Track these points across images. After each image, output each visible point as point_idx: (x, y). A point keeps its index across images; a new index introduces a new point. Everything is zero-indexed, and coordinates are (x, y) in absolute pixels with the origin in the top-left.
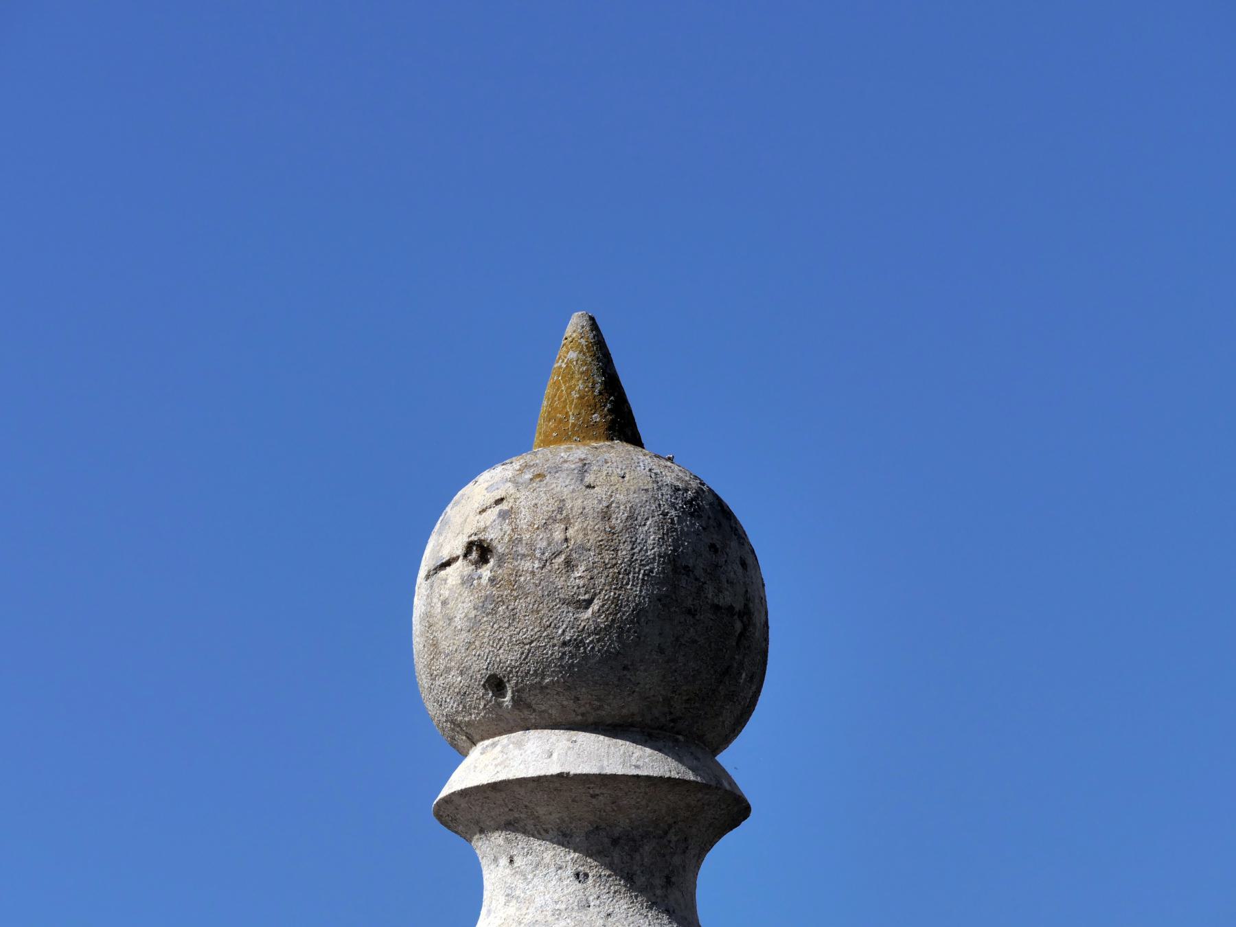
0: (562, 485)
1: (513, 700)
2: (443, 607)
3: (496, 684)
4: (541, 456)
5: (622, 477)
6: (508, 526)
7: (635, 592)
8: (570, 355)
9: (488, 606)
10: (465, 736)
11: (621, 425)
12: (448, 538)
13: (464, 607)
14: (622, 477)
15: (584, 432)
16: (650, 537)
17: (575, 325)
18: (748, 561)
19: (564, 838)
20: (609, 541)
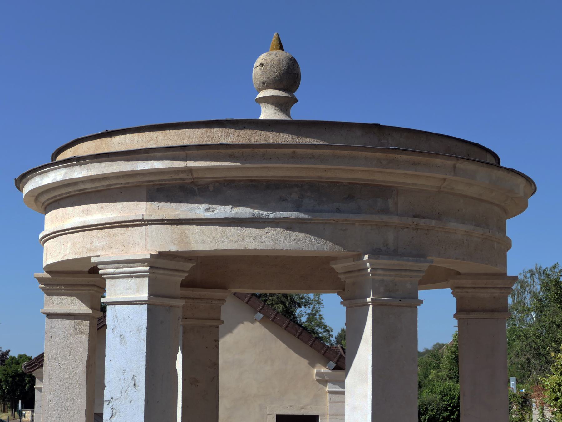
0: (273, 56)
1: (266, 85)
2: (257, 72)
3: (264, 83)
4: (270, 52)
5: (281, 55)
6: (265, 62)
7: (283, 71)
8: (274, 38)
9: (263, 72)
10: (259, 90)
11: (281, 48)
12: (257, 63)
13: (259, 73)
14: (281, 55)
15: (276, 49)
16: (285, 64)
17: (275, 34)
18: (298, 67)
19: (272, 104)
20: (280, 64)
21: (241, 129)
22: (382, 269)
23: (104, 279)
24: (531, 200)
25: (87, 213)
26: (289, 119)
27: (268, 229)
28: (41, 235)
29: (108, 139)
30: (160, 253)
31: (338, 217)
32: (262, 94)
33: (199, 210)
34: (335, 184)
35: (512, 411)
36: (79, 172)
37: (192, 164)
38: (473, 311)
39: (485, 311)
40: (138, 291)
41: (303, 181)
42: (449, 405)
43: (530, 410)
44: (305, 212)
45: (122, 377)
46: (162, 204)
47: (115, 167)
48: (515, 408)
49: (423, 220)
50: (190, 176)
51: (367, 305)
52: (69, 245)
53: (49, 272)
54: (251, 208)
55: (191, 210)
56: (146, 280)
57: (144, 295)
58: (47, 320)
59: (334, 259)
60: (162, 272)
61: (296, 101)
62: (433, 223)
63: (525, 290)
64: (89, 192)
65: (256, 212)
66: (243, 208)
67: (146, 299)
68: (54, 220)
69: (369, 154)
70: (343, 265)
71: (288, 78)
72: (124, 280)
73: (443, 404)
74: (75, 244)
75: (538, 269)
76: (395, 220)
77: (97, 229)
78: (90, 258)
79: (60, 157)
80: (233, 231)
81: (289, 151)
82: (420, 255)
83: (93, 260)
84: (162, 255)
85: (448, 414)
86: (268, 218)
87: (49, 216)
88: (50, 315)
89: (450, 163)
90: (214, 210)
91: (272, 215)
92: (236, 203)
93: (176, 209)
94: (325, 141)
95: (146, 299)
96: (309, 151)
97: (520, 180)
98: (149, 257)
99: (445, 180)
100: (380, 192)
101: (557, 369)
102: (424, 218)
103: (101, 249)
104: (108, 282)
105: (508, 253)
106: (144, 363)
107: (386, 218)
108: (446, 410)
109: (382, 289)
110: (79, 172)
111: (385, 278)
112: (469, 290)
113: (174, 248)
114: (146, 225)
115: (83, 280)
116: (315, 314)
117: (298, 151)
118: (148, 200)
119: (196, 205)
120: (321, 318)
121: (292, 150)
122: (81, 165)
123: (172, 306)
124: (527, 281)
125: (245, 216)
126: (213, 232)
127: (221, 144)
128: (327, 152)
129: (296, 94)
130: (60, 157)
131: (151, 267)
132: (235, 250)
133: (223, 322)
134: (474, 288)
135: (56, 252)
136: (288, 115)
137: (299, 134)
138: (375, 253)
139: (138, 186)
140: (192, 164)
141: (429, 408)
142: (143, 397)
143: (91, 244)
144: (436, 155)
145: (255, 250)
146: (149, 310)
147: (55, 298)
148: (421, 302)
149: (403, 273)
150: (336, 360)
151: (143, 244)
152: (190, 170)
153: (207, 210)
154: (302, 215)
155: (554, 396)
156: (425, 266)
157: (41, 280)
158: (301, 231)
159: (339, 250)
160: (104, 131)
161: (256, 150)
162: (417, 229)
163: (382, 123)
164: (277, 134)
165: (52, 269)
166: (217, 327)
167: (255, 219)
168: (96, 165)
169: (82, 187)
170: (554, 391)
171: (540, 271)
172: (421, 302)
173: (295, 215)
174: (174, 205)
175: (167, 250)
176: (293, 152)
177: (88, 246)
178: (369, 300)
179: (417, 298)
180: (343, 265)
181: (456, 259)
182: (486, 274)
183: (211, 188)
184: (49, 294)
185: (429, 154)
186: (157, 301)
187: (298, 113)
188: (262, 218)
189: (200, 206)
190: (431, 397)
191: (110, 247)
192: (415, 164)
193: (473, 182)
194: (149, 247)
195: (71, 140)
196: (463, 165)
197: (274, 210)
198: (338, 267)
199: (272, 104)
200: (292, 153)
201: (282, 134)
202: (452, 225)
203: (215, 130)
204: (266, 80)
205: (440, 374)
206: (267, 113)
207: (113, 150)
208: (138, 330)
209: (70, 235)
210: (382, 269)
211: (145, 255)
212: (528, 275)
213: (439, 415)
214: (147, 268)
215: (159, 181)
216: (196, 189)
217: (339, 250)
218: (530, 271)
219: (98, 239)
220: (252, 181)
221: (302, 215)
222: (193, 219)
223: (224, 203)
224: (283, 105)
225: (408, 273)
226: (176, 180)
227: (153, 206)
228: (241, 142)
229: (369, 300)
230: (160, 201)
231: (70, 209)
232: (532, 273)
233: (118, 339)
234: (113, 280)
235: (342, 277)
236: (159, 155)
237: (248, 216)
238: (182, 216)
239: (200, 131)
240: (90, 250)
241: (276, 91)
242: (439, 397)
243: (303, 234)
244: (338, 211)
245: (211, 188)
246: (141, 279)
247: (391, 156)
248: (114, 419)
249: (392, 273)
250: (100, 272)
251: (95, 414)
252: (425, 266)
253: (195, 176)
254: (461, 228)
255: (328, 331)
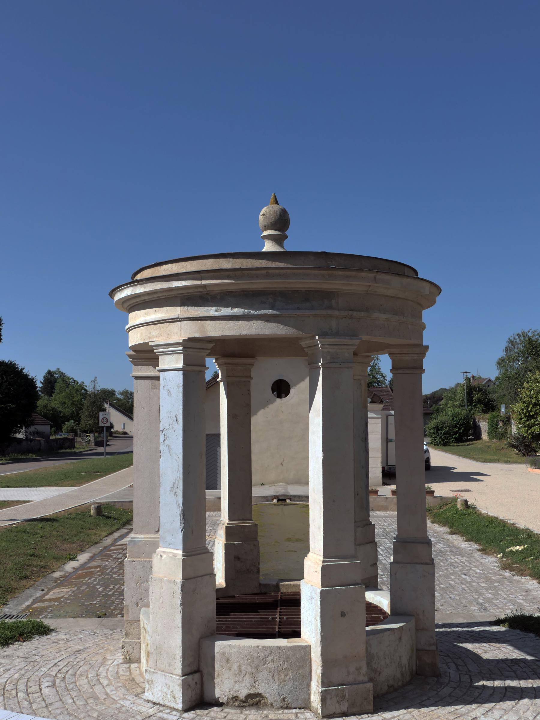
0: (271, 209)
1: (267, 228)
2: (261, 218)
4: (269, 206)
5: (276, 207)
6: (266, 212)
7: (277, 218)
8: (272, 197)
9: (264, 219)
10: (263, 231)
11: (277, 203)
12: (261, 214)
13: (262, 220)
14: (276, 207)
15: (273, 204)
16: (278, 213)
17: (273, 194)
18: (288, 215)
21: (237, 258)
22: (328, 345)
23: (158, 356)
24: (438, 298)
25: (147, 314)
26: (282, 250)
27: (254, 322)
28: (127, 327)
29: (158, 267)
30: (189, 338)
31: (299, 312)
32: (264, 233)
33: (212, 311)
34: (296, 292)
35: (499, 427)
36: (139, 289)
37: (204, 282)
38: (401, 369)
39: (408, 368)
40: (177, 363)
41: (276, 291)
42: (457, 424)
43: (511, 426)
44: (277, 310)
45: (169, 416)
46: (189, 308)
47: (159, 286)
48: (501, 424)
49: (355, 312)
50: (205, 290)
51: (319, 368)
52: (139, 335)
53: (135, 351)
54: (243, 309)
55: (207, 311)
56: (182, 356)
57: (180, 365)
58: (135, 381)
59: (301, 339)
60: (191, 350)
61: (287, 237)
62: (363, 314)
63: (514, 347)
64: (148, 302)
65: (246, 311)
66: (238, 309)
67: (182, 367)
68: (137, 317)
69: (316, 272)
70: (306, 342)
71: (281, 222)
72: (169, 356)
73: (454, 423)
74: (141, 334)
75: (523, 333)
76: (336, 313)
77: (155, 324)
78: (148, 343)
79: (139, 277)
80: (232, 323)
81: (264, 272)
82: (353, 335)
83: (151, 344)
84: (190, 340)
85: (457, 429)
86: (254, 315)
87: (132, 315)
88: (137, 378)
89: (371, 275)
90: (221, 310)
91: (256, 312)
92: (234, 306)
93: (198, 311)
94: (290, 264)
95: (182, 367)
96: (277, 271)
97: (425, 284)
98: (182, 341)
99: (370, 286)
100: (326, 296)
101: (521, 399)
102: (356, 311)
103: (156, 337)
104: (160, 357)
105: (424, 332)
106: (182, 407)
107: (330, 312)
108: (456, 427)
109: (328, 357)
110: (139, 289)
111: (331, 350)
112: (398, 356)
113: (197, 335)
114: (181, 321)
115: (146, 355)
116: (375, 366)
117: (270, 271)
118: (181, 306)
119: (210, 308)
120: (379, 368)
121: (266, 271)
122: (140, 285)
123: (200, 371)
124: (516, 342)
125: (239, 314)
126: (221, 324)
127: (221, 269)
128: (288, 271)
129: (287, 233)
130: (139, 277)
131: (184, 348)
132: (234, 335)
133: (252, 378)
134: (401, 354)
135: (135, 338)
136: (282, 246)
137: (273, 260)
138: (323, 335)
139: (175, 297)
140: (204, 282)
141: (445, 425)
142: (182, 428)
143: (150, 333)
144: (362, 270)
145: (246, 335)
146: (184, 374)
147: (139, 367)
148: (208, 368)
149: (342, 347)
150: (371, 397)
151: (179, 333)
152: (205, 286)
153: (216, 311)
154: (275, 312)
155: (520, 417)
156: (357, 342)
157: (130, 356)
158: (275, 322)
159: (299, 334)
160: (155, 262)
161: (243, 272)
162: (352, 319)
163: (328, 251)
164: (259, 261)
165: (135, 348)
166: (249, 382)
167: (246, 315)
168: (149, 284)
169: (143, 298)
170: (520, 414)
171: (524, 334)
172: (208, 368)
173: (270, 312)
174: (197, 308)
175: (193, 336)
176: (267, 272)
177: (149, 335)
178: (320, 364)
179: (204, 365)
180: (306, 342)
181: (380, 336)
182: (408, 345)
183: (218, 297)
184: (135, 365)
185: (357, 270)
186: (189, 368)
187: (290, 246)
188: (250, 315)
189: (212, 308)
190: (447, 418)
191: (161, 336)
192: (348, 277)
193: (394, 285)
194: (182, 335)
195: (138, 269)
196: (380, 276)
197: (257, 310)
198: (304, 344)
199: (271, 240)
200: (266, 273)
201: (262, 261)
202: (376, 315)
203: (221, 259)
204: (266, 224)
205: (455, 403)
206: (268, 247)
207: (161, 274)
208: (178, 387)
209: (145, 327)
210: (328, 345)
211: (180, 340)
212: (517, 337)
213: (451, 430)
214: (181, 348)
215: (187, 293)
216: (209, 297)
217: (299, 334)
218: (518, 335)
219: (154, 330)
220: (243, 291)
221: (275, 312)
222: (208, 317)
223: (226, 306)
224: (278, 240)
225: (345, 347)
226: (197, 292)
227: (184, 309)
228: (237, 267)
229: (320, 364)
230: (188, 306)
231: (138, 312)
232: (519, 335)
233: (167, 393)
234: (163, 356)
235: (306, 350)
236: (184, 277)
237: (241, 314)
238: (201, 315)
239: (211, 261)
240: (150, 338)
241: (270, 231)
242: (451, 418)
243: (276, 324)
244: (299, 308)
245: (218, 297)
246: (178, 355)
247: (331, 272)
248: (166, 441)
249: (335, 347)
250: (155, 351)
251: (207, 435)
252: (357, 342)
253: (208, 289)
254: (382, 316)
255: (384, 377)
